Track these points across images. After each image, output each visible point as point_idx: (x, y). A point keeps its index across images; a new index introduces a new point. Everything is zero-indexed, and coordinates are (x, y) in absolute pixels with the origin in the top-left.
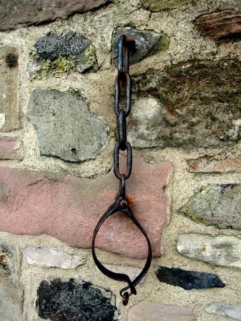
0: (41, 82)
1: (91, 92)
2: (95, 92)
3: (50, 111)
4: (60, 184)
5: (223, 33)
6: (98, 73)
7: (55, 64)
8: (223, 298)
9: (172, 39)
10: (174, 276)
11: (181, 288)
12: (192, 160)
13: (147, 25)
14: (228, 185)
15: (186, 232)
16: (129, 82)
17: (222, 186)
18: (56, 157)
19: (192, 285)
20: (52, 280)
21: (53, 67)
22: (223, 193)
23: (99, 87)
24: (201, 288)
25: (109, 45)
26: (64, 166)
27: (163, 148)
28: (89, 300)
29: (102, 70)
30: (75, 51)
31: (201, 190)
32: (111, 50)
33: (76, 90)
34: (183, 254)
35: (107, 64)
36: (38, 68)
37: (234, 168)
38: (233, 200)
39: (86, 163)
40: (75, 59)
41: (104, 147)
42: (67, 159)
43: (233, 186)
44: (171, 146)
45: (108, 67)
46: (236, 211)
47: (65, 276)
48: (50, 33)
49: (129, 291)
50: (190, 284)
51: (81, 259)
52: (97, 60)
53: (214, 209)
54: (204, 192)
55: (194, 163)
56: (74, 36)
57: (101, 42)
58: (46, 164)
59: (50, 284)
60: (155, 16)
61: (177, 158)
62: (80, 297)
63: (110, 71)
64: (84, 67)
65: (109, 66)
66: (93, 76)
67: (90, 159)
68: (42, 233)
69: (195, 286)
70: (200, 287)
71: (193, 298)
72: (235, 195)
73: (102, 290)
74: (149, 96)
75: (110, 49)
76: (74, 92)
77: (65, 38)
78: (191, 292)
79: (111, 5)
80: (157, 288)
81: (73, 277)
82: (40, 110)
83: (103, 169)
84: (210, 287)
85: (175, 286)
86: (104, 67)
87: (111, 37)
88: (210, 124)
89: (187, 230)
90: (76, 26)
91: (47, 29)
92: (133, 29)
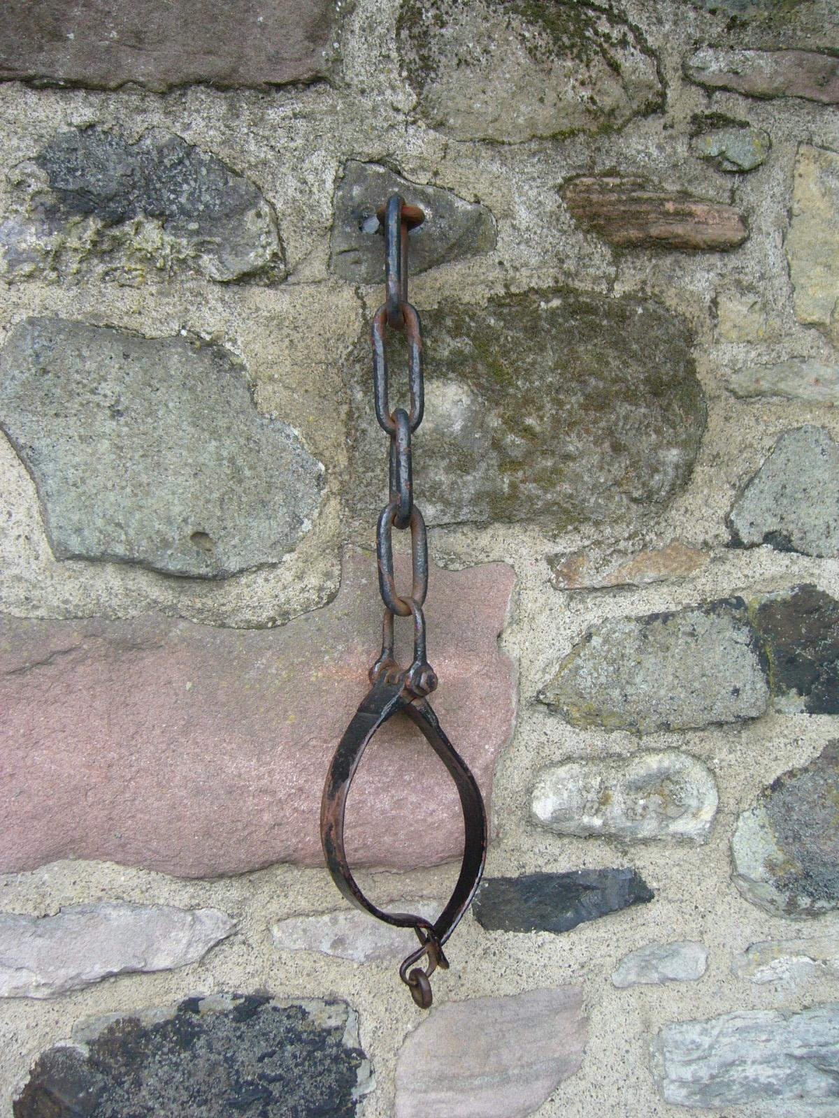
0: (59, 292)
1: (257, 347)
2: (274, 350)
3: (96, 398)
4: (149, 659)
5: (633, 234)
6: (283, 291)
7: (114, 238)
8: (652, 931)
9: (504, 226)
10: (526, 901)
11: (547, 933)
12: (563, 555)
13: (436, 174)
14: (654, 617)
15: (557, 758)
16: (416, 332)
17: (638, 619)
18: (128, 563)
19: (577, 912)
20: (96, 1036)
21: (105, 247)
22: (646, 637)
23: (288, 336)
24: (606, 914)
25: (327, 211)
26: (159, 592)
27: (481, 526)
28: (261, 1060)
29: (298, 283)
30: (201, 207)
31: (589, 637)
32: (332, 228)
33: (208, 338)
34: (556, 829)
35: (317, 268)
36: (52, 242)
37: (664, 572)
38: (669, 654)
39: (243, 580)
40: (197, 233)
41: (307, 526)
42: (173, 566)
43: (666, 617)
44: (509, 520)
45: (319, 277)
46: (676, 682)
47: (157, 1001)
48: (91, 126)
49: (423, 964)
50: (569, 914)
51: (225, 918)
52: (283, 250)
53: (628, 682)
54: (596, 641)
55: (568, 565)
56: (188, 155)
57: (298, 196)
58: (85, 589)
59: (84, 1051)
60: (459, 151)
61: (524, 551)
62: (226, 1059)
63: (323, 289)
64: (238, 265)
65: (325, 275)
66: (264, 298)
67: (262, 565)
68: (48, 858)
69: (584, 913)
70: (604, 911)
71: (580, 953)
72: (672, 641)
73: (310, 1007)
74: (451, 375)
75: (328, 224)
76: (198, 343)
77: (154, 153)
78: (573, 936)
79: (321, 87)
80: (480, 951)
81: (193, 994)
82: (58, 392)
83: (306, 595)
84: (627, 904)
85: (528, 930)
86: (306, 272)
87: (329, 185)
88: (608, 459)
89: (558, 753)
90: (198, 123)
91: (81, 110)
92: (394, 176)
